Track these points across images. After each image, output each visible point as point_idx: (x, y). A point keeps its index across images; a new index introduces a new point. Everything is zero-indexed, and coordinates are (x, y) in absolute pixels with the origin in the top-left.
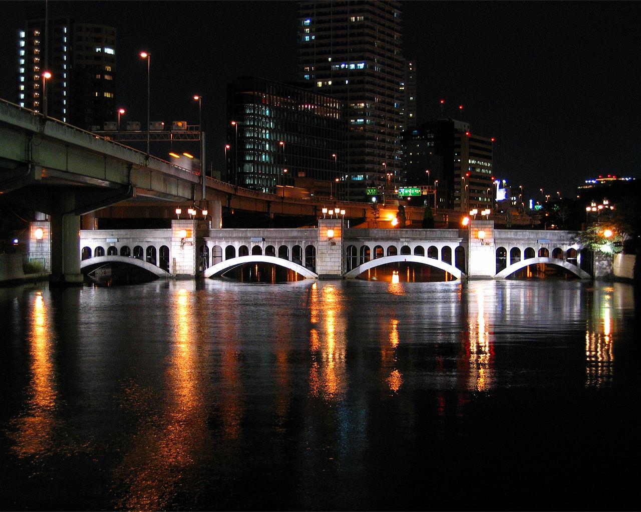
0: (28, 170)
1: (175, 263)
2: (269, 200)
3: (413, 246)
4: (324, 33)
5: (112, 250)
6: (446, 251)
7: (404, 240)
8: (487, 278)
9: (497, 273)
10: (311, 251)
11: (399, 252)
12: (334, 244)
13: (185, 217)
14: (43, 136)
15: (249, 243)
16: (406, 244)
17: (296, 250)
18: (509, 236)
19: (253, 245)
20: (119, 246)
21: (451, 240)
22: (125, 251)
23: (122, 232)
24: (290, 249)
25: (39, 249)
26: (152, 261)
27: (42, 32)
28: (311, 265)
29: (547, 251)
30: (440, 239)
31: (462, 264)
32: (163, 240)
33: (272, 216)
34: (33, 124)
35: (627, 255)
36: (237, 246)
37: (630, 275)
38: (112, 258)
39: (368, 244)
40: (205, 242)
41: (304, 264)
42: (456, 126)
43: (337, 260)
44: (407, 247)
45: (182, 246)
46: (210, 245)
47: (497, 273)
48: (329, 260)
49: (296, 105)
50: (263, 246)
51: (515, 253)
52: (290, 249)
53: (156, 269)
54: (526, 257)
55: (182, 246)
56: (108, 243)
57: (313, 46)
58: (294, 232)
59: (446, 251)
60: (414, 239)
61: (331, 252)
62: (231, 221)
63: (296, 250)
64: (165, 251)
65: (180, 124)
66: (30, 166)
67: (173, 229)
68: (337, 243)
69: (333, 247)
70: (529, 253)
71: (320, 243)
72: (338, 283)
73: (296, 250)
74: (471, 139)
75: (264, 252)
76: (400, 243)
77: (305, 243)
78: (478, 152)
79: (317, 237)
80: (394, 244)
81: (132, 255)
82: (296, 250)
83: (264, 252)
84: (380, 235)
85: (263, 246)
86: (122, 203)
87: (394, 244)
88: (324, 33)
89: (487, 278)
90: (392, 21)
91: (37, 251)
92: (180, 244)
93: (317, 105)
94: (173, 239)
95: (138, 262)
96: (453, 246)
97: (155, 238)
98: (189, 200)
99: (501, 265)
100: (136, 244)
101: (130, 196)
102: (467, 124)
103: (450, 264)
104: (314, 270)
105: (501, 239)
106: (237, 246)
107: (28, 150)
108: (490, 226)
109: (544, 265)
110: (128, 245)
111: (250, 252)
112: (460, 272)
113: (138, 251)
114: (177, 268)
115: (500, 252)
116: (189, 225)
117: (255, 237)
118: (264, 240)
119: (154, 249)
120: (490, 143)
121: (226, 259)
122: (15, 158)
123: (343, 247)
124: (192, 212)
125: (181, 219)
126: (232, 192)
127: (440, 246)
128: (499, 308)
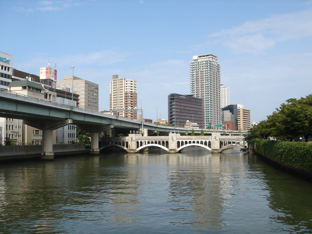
1: (129, 146)
10: (167, 142)
19: (151, 141)
24: (161, 142)
28: (167, 146)
30: (204, 139)
34: (68, 108)
45: (132, 141)
51: (182, 142)
52: (161, 142)
55: (132, 141)
63: (163, 142)
75: (154, 143)
78: (73, 103)
82: (163, 142)
83: (154, 143)
87: (190, 140)
95: (120, 146)
103: (207, 146)
106: (188, 141)
121: (185, 144)
127: (204, 141)
128: (23, 173)
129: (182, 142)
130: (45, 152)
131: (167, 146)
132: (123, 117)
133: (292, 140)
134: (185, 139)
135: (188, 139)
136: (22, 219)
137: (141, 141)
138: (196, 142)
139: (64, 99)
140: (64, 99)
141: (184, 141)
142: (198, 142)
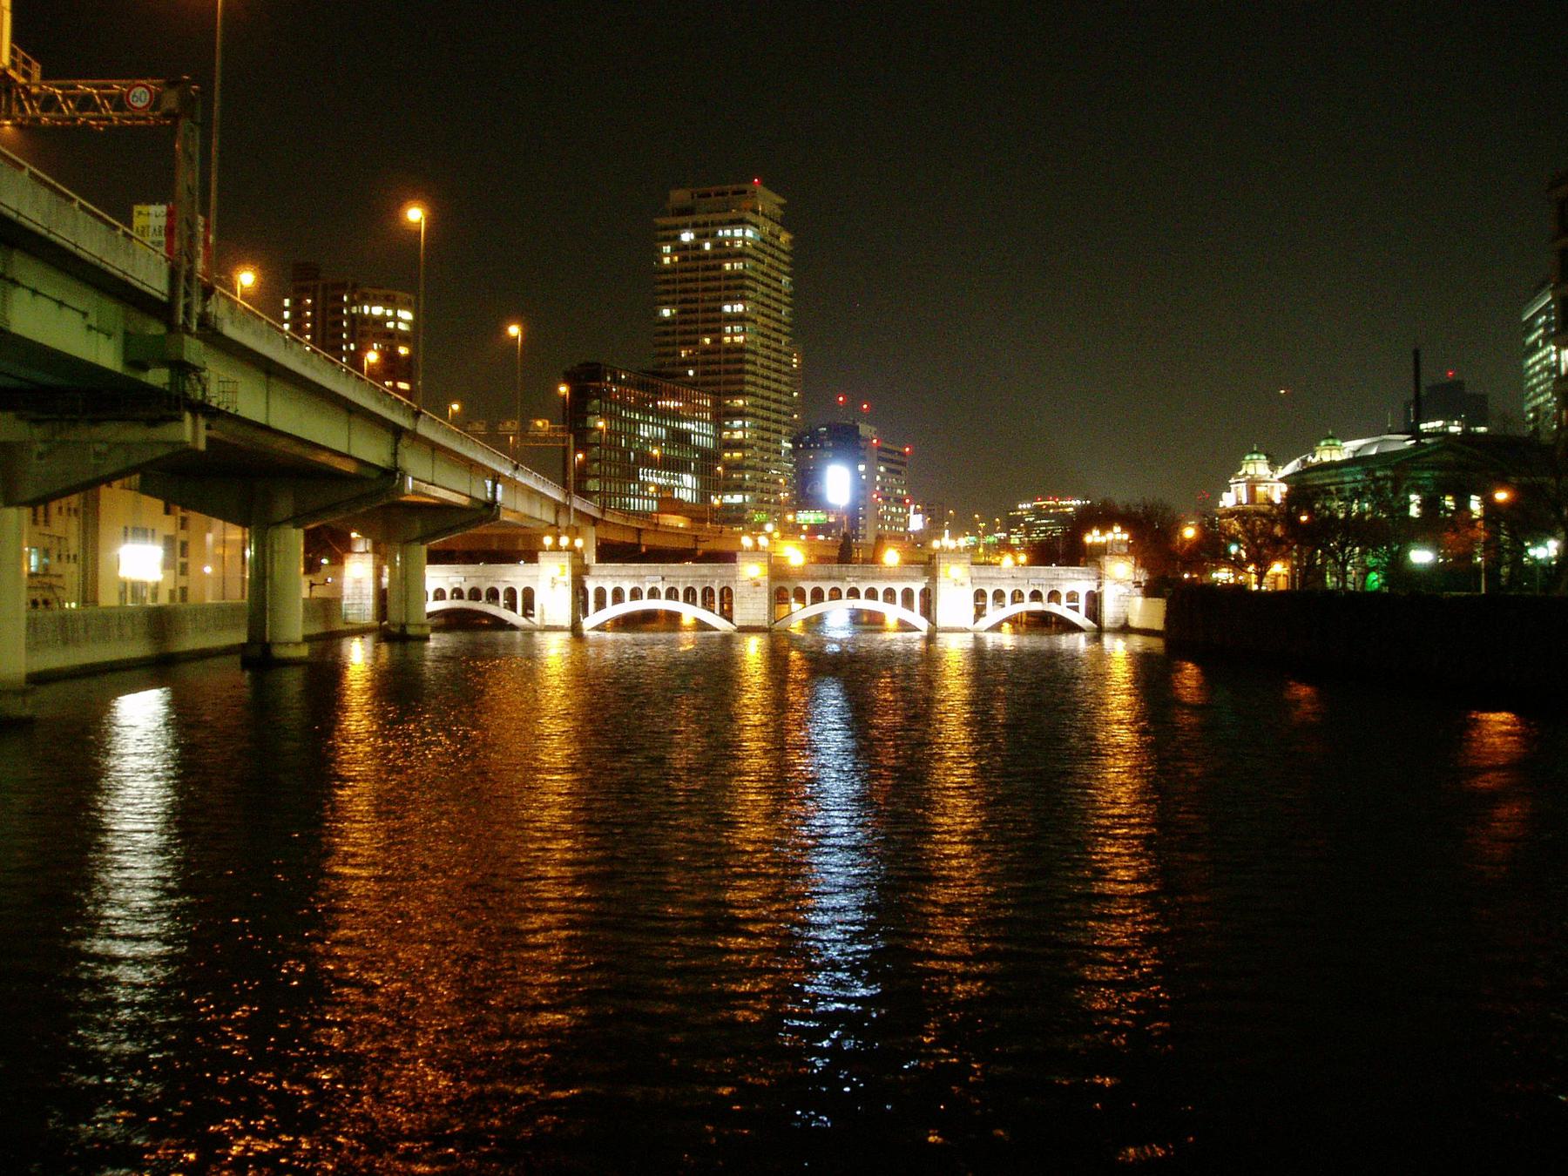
0: (394, 482)
2: (639, 526)
3: (863, 588)
4: (688, 306)
5: (458, 593)
6: (908, 595)
7: (851, 579)
8: (967, 631)
9: (975, 622)
10: (727, 594)
11: (844, 595)
12: (758, 585)
13: (556, 548)
14: (415, 437)
15: (644, 583)
16: (854, 585)
17: (908, 594)
18: (991, 575)
20: (466, 588)
21: (913, 579)
22: (475, 594)
23: (471, 568)
25: (357, 591)
26: (513, 607)
27: (314, 299)
28: (727, 615)
29: (677, 591)
31: (928, 610)
32: (526, 579)
33: (644, 550)
35: (1150, 599)
36: (627, 587)
37: (1159, 625)
38: (457, 604)
39: (803, 584)
40: (583, 582)
41: (717, 612)
42: (861, 432)
43: (762, 606)
44: (1038, 591)
46: (591, 585)
47: (975, 622)
48: (751, 606)
49: (655, 401)
50: (663, 588)
51: (999, 595)
53: (516, 618)
54: (1014, 601)
56: (452, 584)
57: (674, 323)
58: (705, 568)
59: (908, 595)
60: (864, 578)
61: (754, 595)
62: (608, 553)
63: (708, 592)
64: (529, 594)
65: (540, 423)
66: (398, 475)
67: (541, 563)
68: (761, 583)
69: (758, 588)
70: (1036, 596)
71: (739, 584)
72: (369, 639)
73: (708, 592)
74: (880, 449)
75: (663, 595)
76: (845, 584)
77: (719, 583)
79: (734, 576)
80: (837, 584)
81: (484, 598)
84: (819, 573)
85: (663, 588)
86: (482, 530)
87: (837, 584)
88: (688, 306)
89: (967, 631)
90: (780, 291)
91: (354, 594)
92: (550, 584)
93: (682, 401)
94: (540, 578)
95: (491, 609)
96: (917, 587)
97: (516, 576)
98: (551, 525)
99: (980, 613)
100: (490, 585)
101: (496, 518)
102: (874, 429)
104: (730, 620)
105: (980, 578)
106: (627, 587)
107: (395, 454)
108: (965, 561)
109: (1024, 615)
110: (480, 587)
111: (645, 595)
112: (926, 622)
113: (493, 595)
114: (546, 617)
115: (980, 595)
116: (562, 559)
117: (650, 576)
118: (663, 579)
119: (712, 591)
120: (904, 454)
121: (812, 604)
122: (381, 464)
123: (770, 589)
124: (564, 541)
125: (551, 550)
126: (598, 515)
129: (999, 595)
130: (268, 638)
131: (727, 615)
132: (1092, 586)
133: (168, 945)
134: (814, 579)
135: (830, 578)
136: (1020, 837)
137: (600, 585)
138: (862, 595)
139: (349, 448)
140: (349, 448)
141: (609, 589)
142: (1054, 596)
